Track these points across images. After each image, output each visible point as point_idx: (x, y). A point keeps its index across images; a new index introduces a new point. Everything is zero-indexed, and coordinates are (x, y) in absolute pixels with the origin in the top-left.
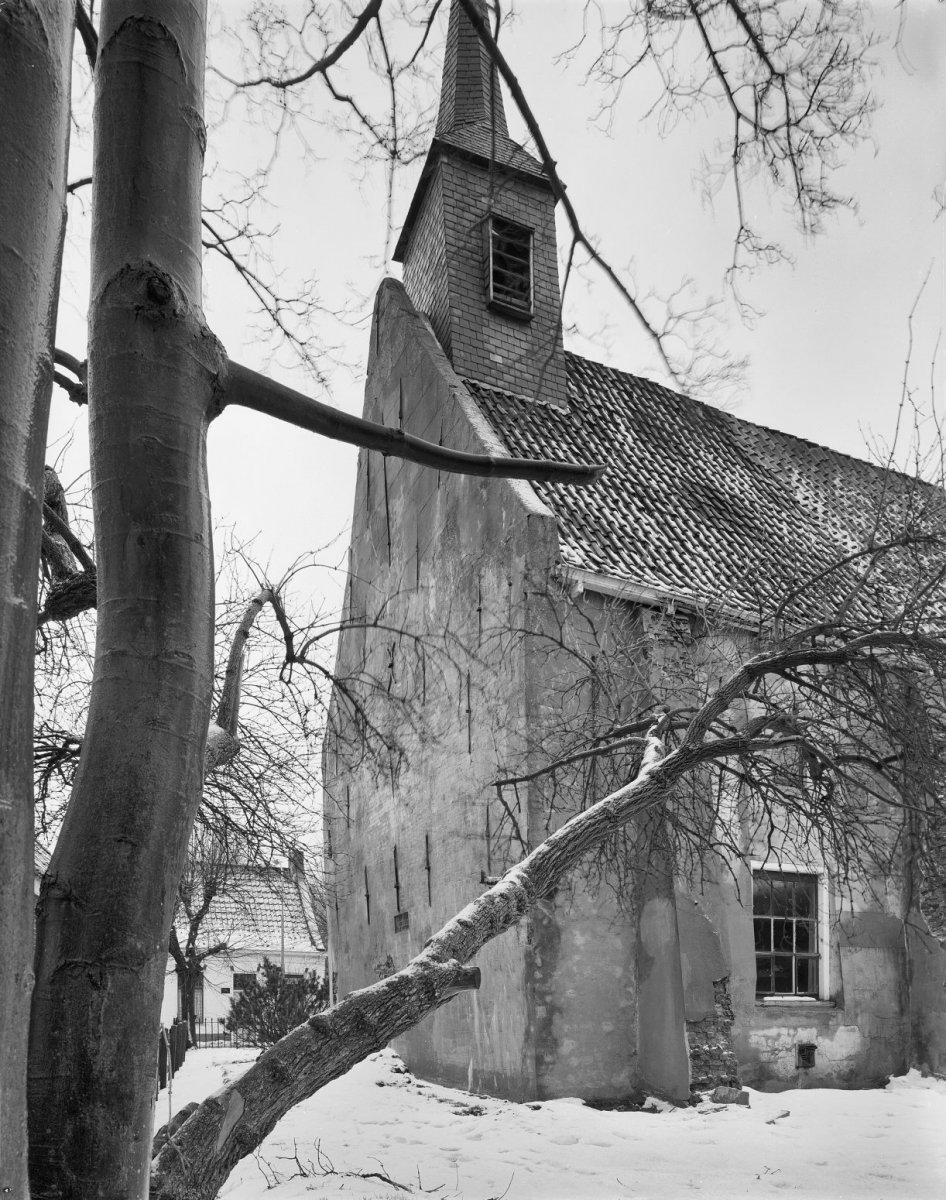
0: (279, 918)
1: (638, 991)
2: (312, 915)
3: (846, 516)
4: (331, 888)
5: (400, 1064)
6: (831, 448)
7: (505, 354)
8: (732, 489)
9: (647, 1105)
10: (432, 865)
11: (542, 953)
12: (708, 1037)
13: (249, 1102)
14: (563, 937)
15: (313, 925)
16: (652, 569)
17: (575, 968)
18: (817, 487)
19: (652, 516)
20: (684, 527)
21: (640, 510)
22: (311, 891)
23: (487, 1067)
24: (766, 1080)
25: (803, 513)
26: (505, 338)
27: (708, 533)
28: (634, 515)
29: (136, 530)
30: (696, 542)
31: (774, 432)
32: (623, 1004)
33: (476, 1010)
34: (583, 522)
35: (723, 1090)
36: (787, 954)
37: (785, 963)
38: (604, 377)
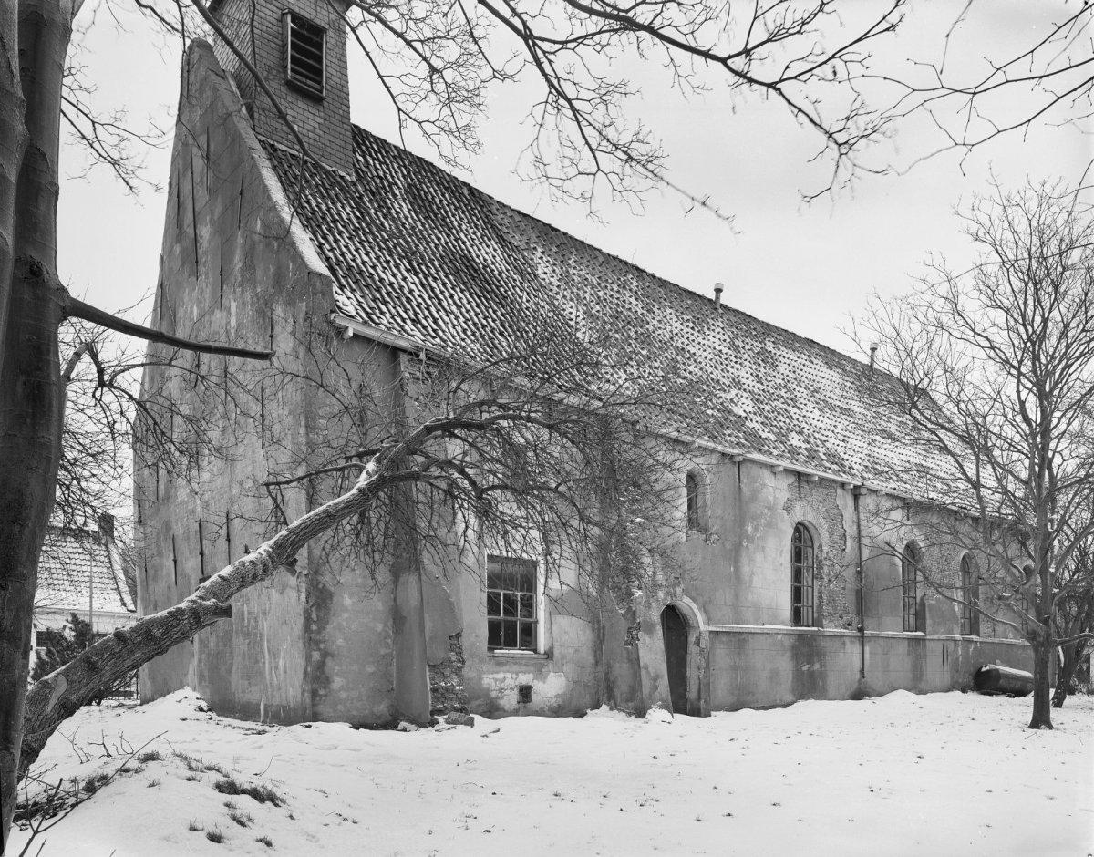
0: (87, 579)
1: (395, 642)
2: (123, 577)
3: (575, 290)
4: (140, 553)
5: (204, 704)
6: (571, 233)
7: (301, 124)
8: (485, 260)
9: (400, 727)
10: (231, 537)
11: (316, 609)
12: (444, 677)
13: (70, 682)
14: (335, 598)
15: (124, 587)
16: (413, 320)
17: (344, 623)
18: (555, 265)
19: (418, 277)
20: (443, 288)
21: (408, 270)
22: (123, 556)
23: (276, 701)
24: (493, 711)
25: (541, 286)
26: (301, 111)
27: (461, 295)
28: (402, 274)
29: (22, 378)
30: (451, 301)
31: (525, 216)
32: (383, 651)
33: (267, 657)
34: (358, 277)
35: (454, 715)
36: (513, 619)
37: (510, 626)
38: (386, 152)
